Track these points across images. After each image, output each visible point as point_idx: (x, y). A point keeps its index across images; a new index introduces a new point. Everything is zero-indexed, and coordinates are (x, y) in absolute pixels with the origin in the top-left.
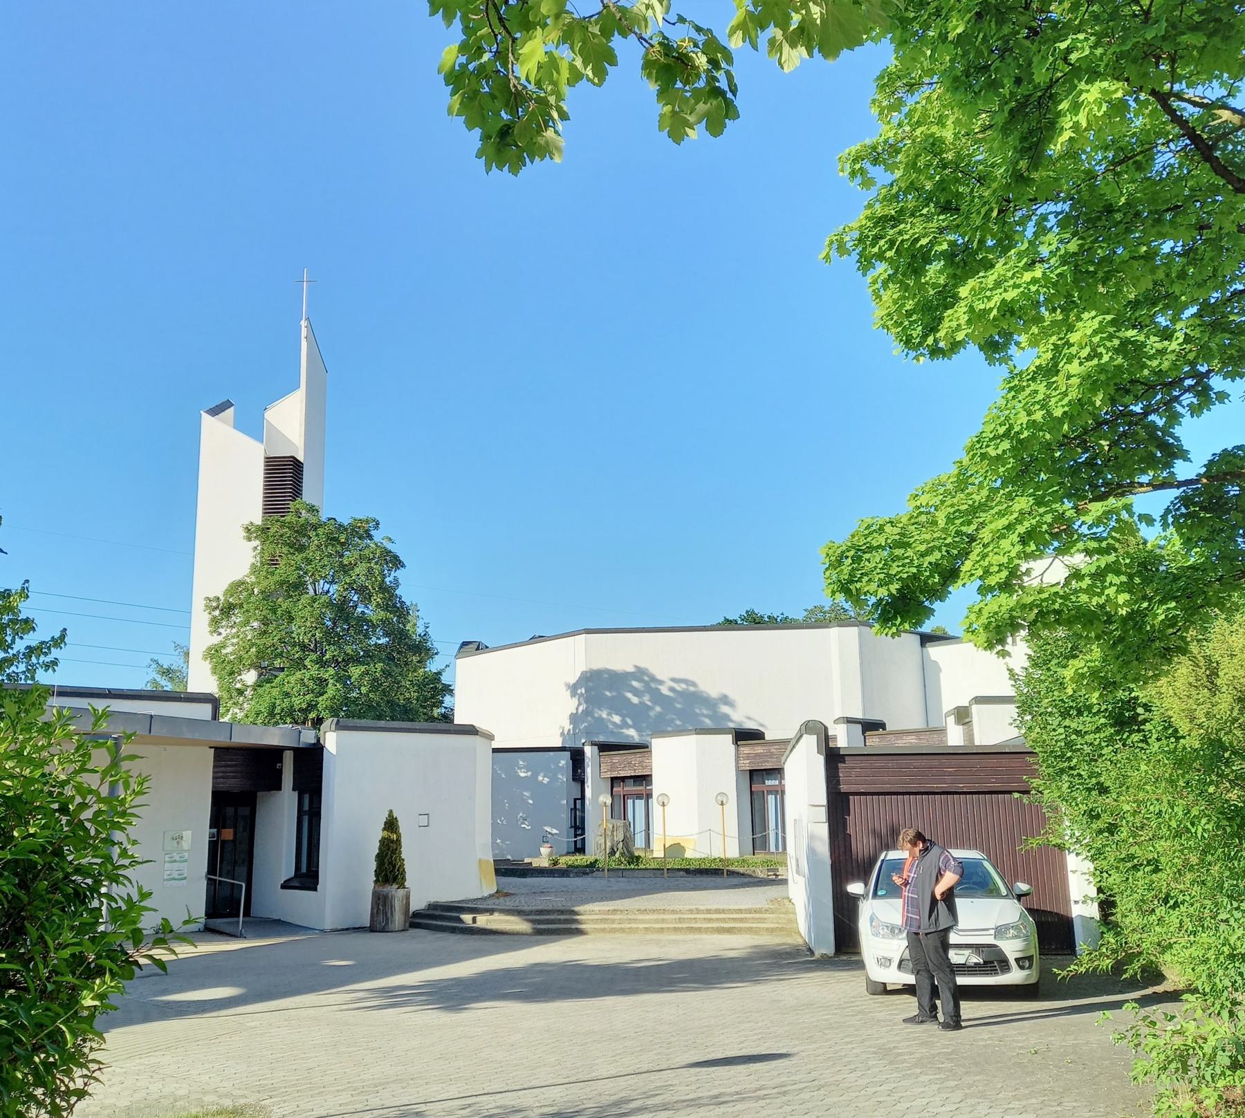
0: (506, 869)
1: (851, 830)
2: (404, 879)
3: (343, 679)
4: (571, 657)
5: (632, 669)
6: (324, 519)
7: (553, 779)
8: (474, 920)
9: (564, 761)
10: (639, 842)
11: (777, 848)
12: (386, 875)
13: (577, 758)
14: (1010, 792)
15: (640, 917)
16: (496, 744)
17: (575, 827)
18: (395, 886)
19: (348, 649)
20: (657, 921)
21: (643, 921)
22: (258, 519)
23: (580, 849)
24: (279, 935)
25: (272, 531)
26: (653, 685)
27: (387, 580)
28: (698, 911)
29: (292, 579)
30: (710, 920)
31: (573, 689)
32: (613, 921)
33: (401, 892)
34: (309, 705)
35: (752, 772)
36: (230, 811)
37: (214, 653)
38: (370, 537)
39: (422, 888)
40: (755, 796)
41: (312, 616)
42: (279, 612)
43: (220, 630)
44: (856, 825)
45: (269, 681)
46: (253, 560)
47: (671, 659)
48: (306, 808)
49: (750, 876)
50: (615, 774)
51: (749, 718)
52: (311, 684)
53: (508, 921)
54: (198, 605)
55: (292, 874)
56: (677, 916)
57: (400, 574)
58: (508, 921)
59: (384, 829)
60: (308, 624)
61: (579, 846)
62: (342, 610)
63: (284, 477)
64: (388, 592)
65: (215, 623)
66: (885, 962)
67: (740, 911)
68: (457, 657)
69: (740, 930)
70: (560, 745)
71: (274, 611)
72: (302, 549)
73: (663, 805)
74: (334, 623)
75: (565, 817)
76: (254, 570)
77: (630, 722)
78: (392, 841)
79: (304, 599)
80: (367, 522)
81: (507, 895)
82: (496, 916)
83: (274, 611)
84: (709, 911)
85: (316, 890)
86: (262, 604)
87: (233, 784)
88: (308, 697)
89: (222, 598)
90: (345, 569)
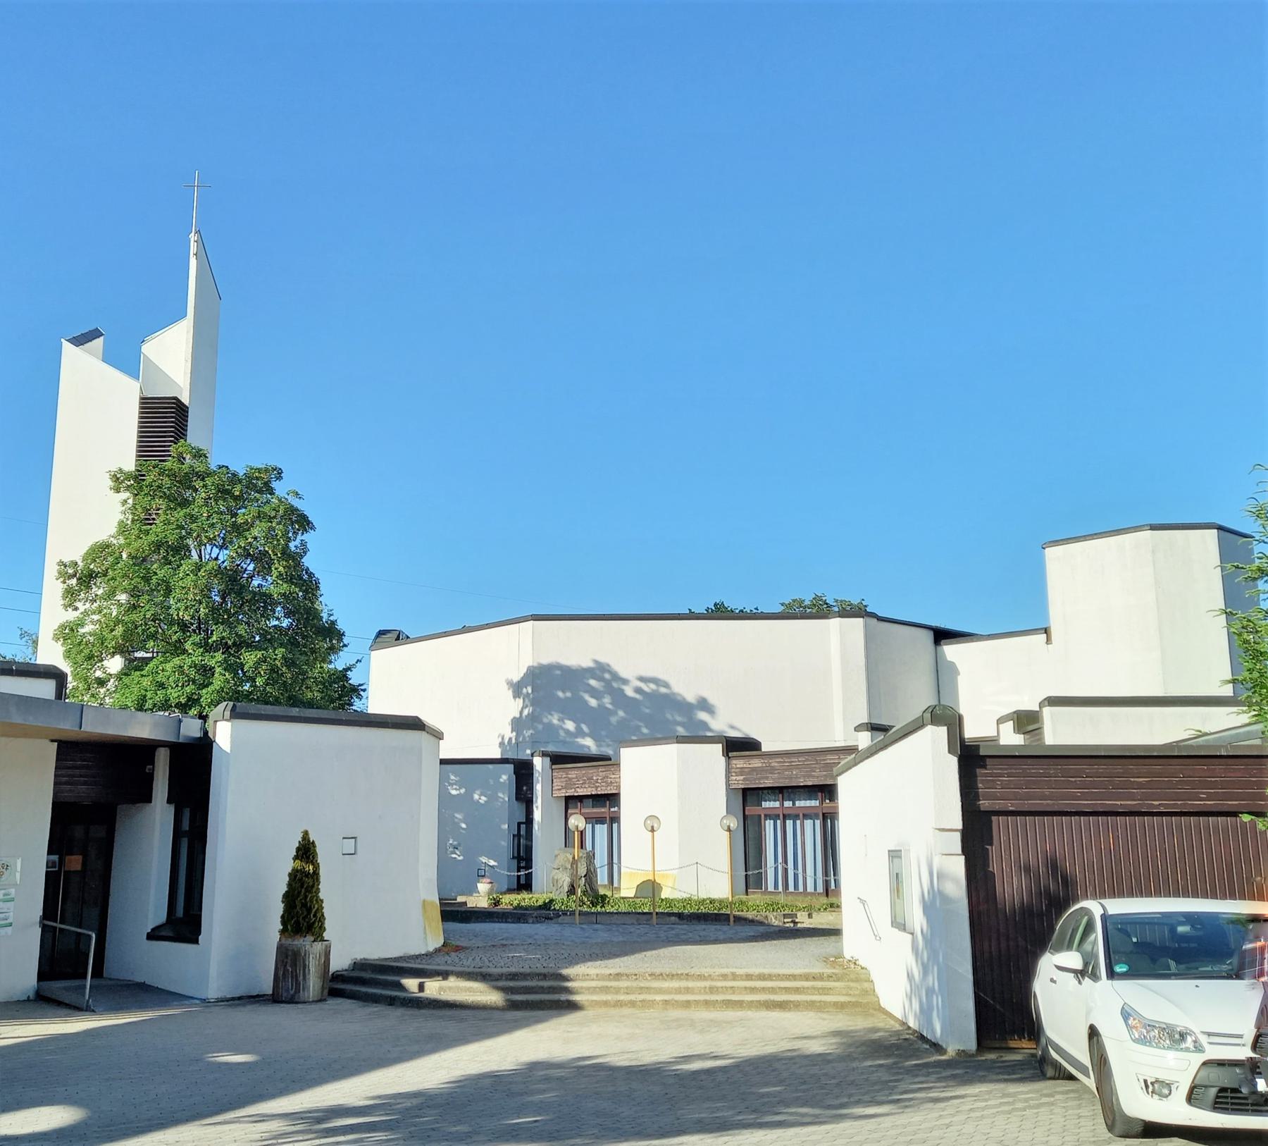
0: (452, 913)
1: (994, 867)
2: (322, 928)
3: (233, 667)
4: (517, 649)
5: (591, 665)
6: (213, 467)
7: (492, 798)
8: (421, 987)
9: (506, 776)
10: (602, 878)
11: (776, 886)
12: (297, 923)
13: (523, 772)
14: (1234, 814)
15: (656, 984)
16: (448, 750)
17: (518, 858)
18: (310, 938)
19: (242, 629)
20: (679, 991)
21: (660, 991)
22: (130, 465)
23: (525, 885)
24: (142, 1006)
25: (149, 479)
26: (615, 685)
27: (292, 545)
28: (735, 977)
29: (172, 539)
30: (753, 990)
31: (517, 689)
32: (617, 990)
33: (318, 947)
34: (189, 699)
35: (745, 792)
36: (78, 832)
37: (67, 633)
38: (271, 491)
39: (348, 939)
40: (749, 822)
41: (196, 586)
42: (154, 581)
43: (78, 604)
44: (1000, 860)
45: (138, 669)
46: (122, 517)
47: (641, 653)
48: (186, 826)
49: (761, 923)
50: (570, 793)
51: (732, 727)
52: (193, 673)
53: (469, 990)
54: (51, 570)
55: (162, 917)
56: (707, 984)
57: (308, 537)
58: (469, 990)
59: (296, 858)
60: (191, 596)
61: (523, 881)
62: (232, 581)
63: (164, 420)
64: (294, 559)
65: (70, 596)
66: (1157, 1088)
67: (793, 977)
68: (372, 648)
69: (796, 1006)
70: (498, 756)
71: (147, 579)
72: (185, 503)
73: (653, 830)
74: (223, 598)
75: (505, 845)
76: (123, 529)
77: (584, 727)
78: (307, 875)
79: (186, 566)
80: (266, 470)
81: (458, 949)
82: (452, 982)
83: (147, 579)
84: (749, 977)
85: (196, 941)
86: (133, 566)
87: (83, 792)
88: (188, 689)
89: (80, 564)
90: (240, 530)
